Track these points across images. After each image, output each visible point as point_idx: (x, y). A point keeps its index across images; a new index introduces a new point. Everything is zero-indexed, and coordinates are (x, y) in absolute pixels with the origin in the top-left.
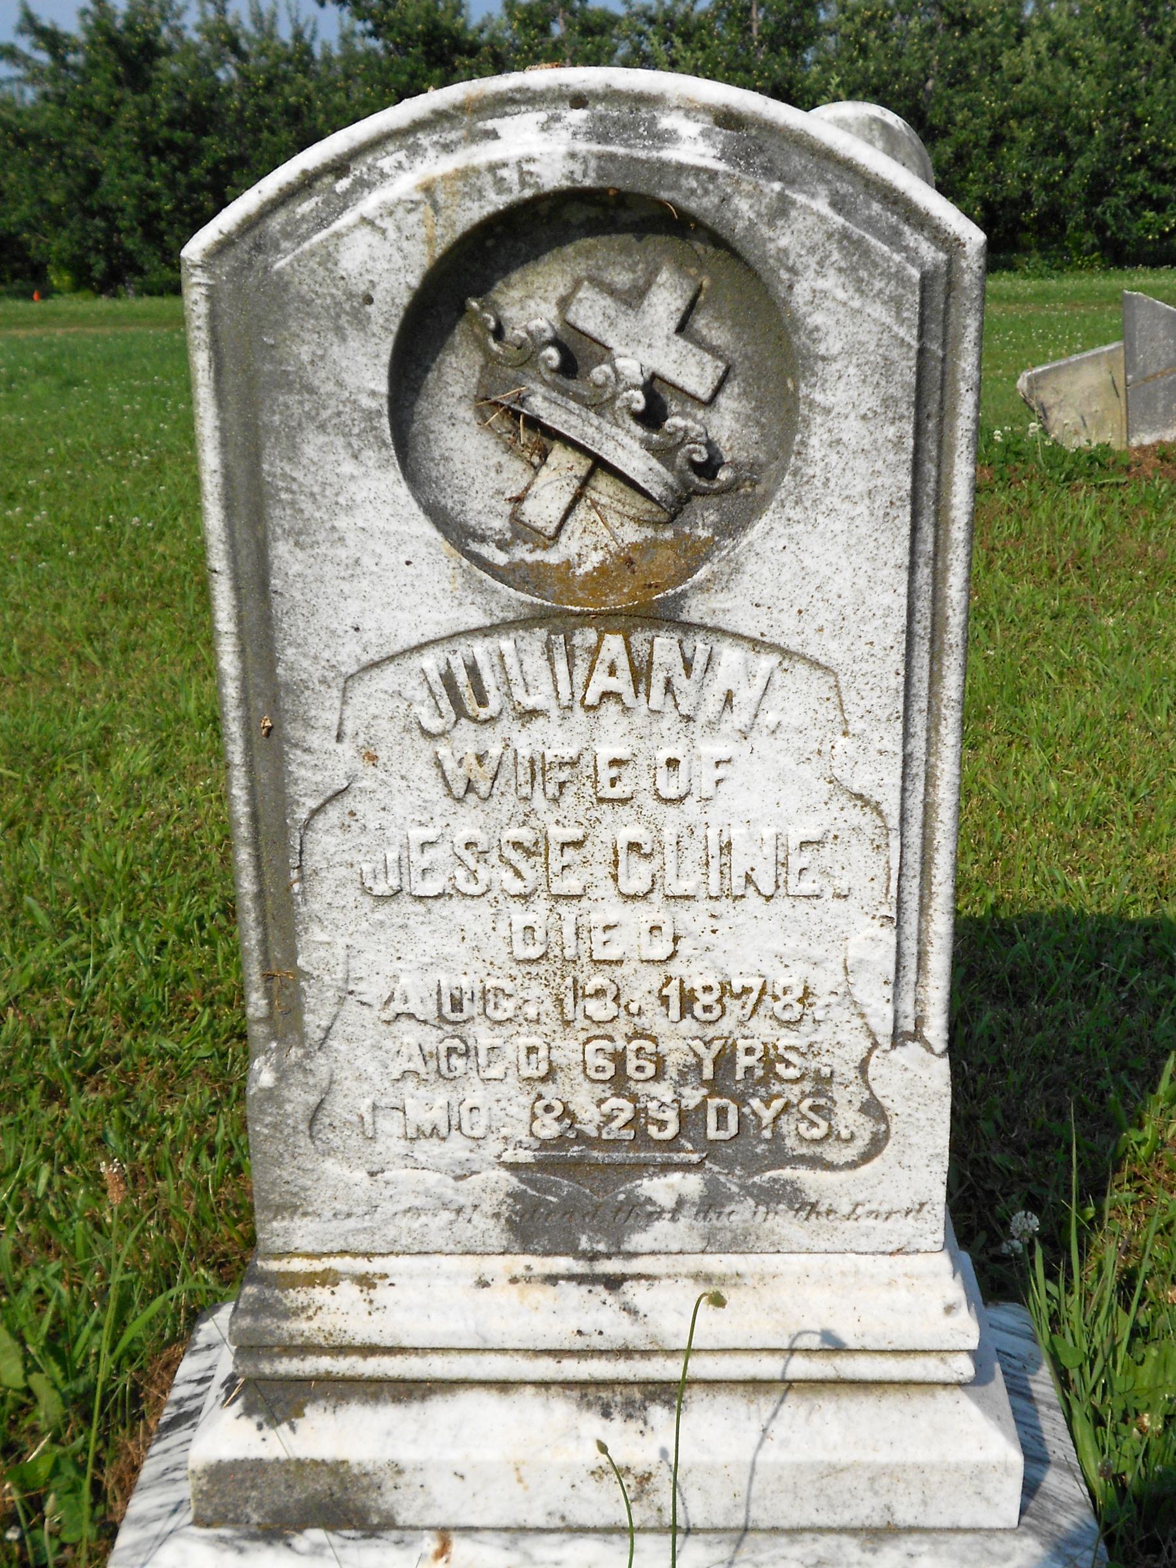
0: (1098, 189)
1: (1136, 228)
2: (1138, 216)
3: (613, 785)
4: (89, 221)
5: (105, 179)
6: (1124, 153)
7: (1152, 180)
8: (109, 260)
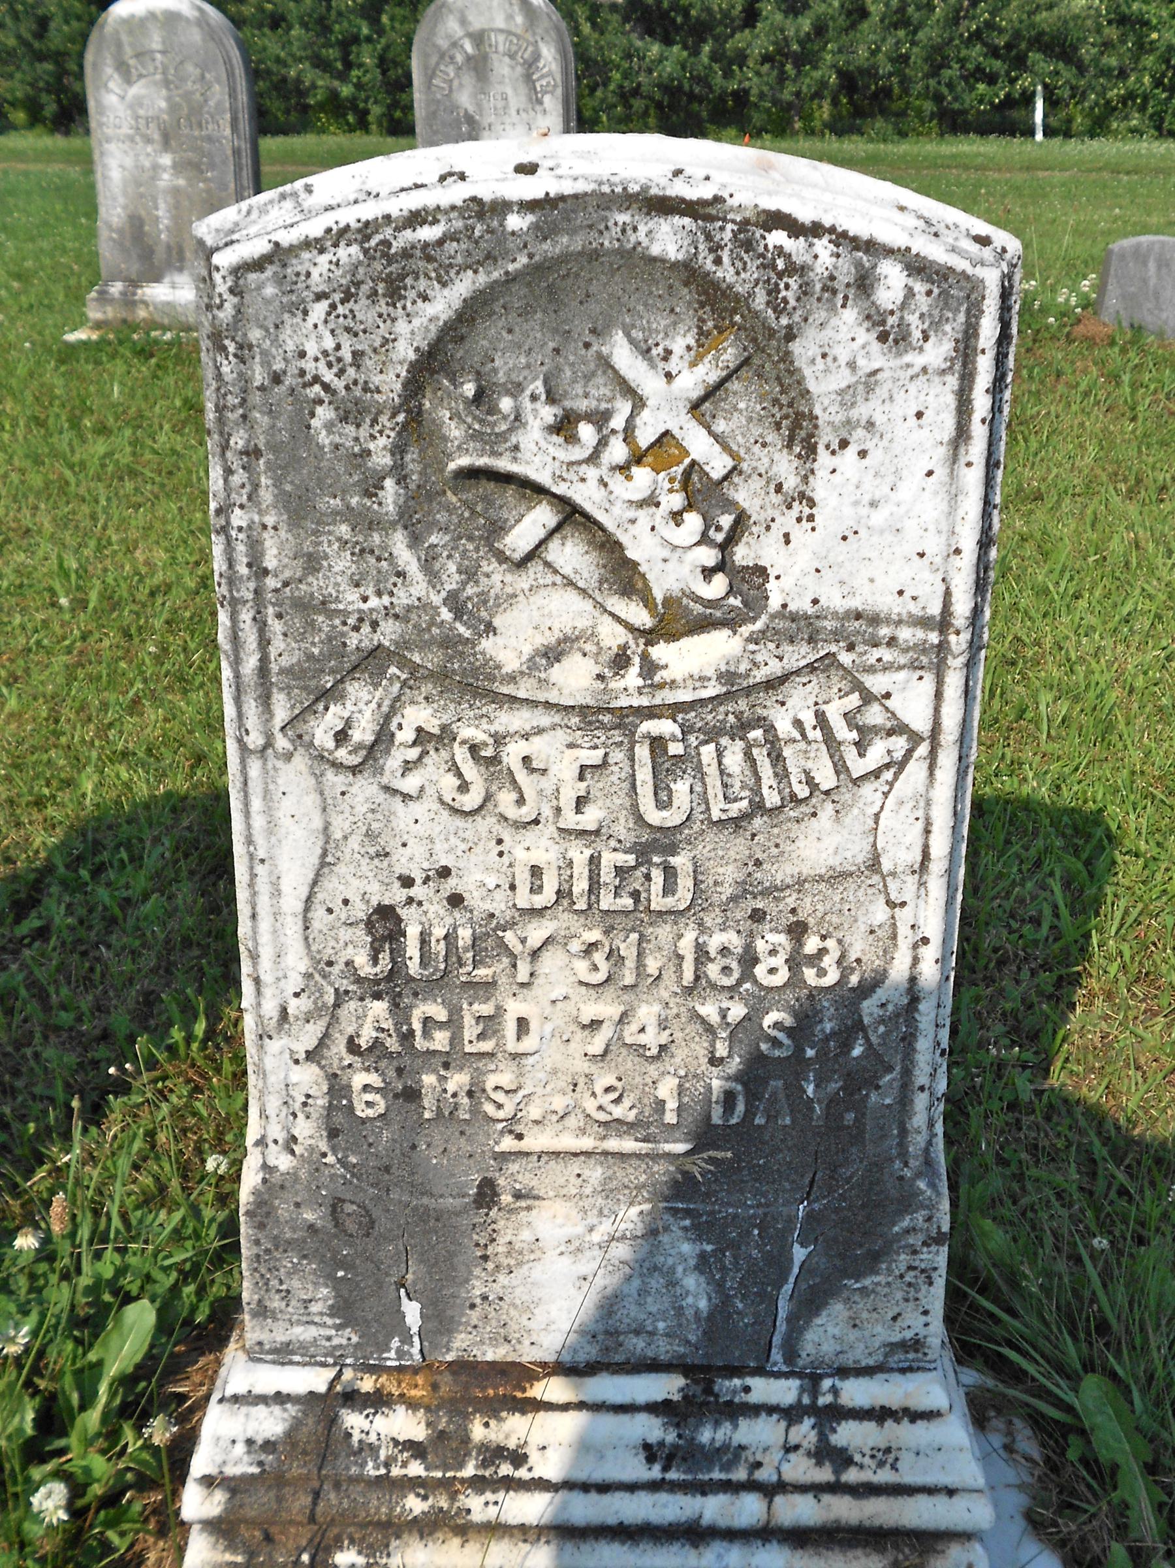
0: (937, 61)
1: (969, 99)
2: (972, 88)
3: (578, 810)
4: (37, 65)
5: (53, 25)
6: (961, 29)
7: (985, 56)
8: (59, 101)
